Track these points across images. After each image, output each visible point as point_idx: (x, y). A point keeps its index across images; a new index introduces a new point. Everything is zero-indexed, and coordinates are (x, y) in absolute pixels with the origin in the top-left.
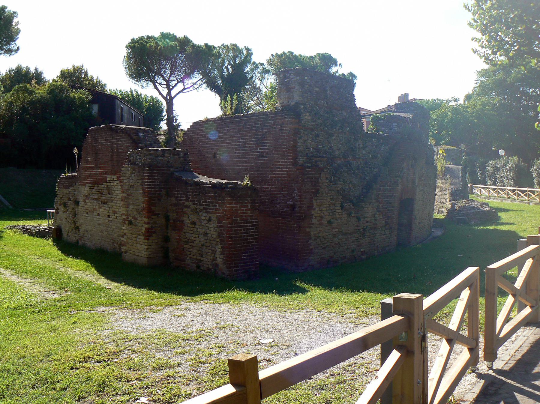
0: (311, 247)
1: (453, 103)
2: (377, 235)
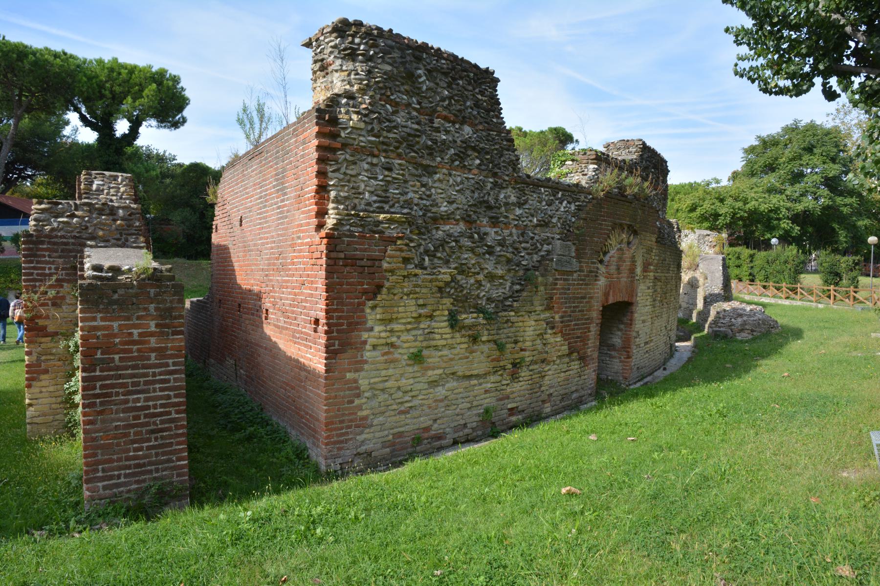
0: (365, 413)
1: (714, 185)
2: (550, 373)
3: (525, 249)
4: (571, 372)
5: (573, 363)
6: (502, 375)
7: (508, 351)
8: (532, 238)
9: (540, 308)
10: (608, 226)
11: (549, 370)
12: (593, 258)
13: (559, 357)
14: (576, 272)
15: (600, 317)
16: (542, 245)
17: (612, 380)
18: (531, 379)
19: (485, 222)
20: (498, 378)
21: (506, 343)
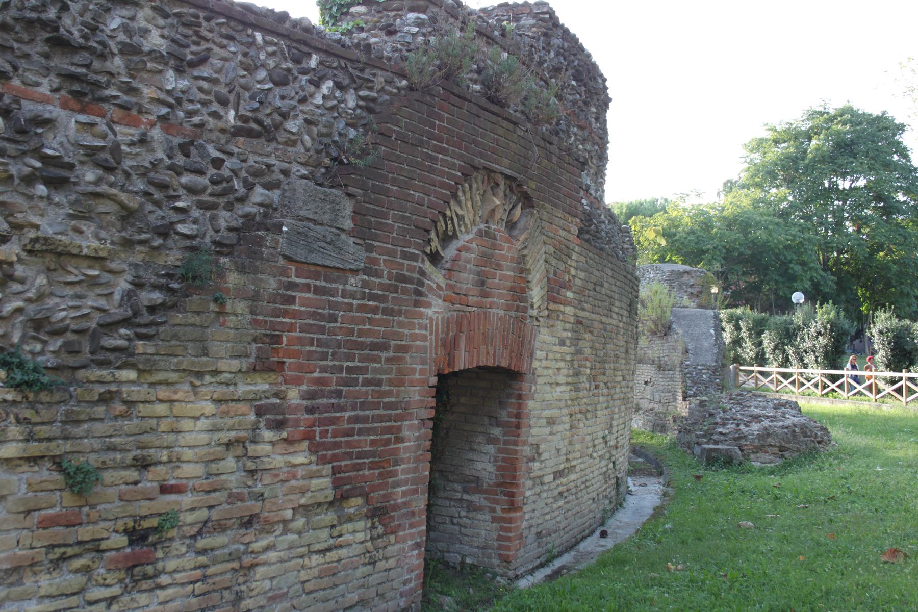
2: (272, 555)
3: (191, 190)
4: (343, 552)
5: (349, 526)
6: (86, 570)
7: (112, 492)
8: (217, 163)
9: (235, 364)
10: (452, 166)
11: (267, 549)
12: (408, 244)
13: (305, 510)
14: (355, 272)
15: (432, 402)
16: (250, 187)
17: (473, 566)
18: (204, 578)
19: (44, 89)
20: (74, 581)
21: (104, 467)
